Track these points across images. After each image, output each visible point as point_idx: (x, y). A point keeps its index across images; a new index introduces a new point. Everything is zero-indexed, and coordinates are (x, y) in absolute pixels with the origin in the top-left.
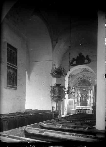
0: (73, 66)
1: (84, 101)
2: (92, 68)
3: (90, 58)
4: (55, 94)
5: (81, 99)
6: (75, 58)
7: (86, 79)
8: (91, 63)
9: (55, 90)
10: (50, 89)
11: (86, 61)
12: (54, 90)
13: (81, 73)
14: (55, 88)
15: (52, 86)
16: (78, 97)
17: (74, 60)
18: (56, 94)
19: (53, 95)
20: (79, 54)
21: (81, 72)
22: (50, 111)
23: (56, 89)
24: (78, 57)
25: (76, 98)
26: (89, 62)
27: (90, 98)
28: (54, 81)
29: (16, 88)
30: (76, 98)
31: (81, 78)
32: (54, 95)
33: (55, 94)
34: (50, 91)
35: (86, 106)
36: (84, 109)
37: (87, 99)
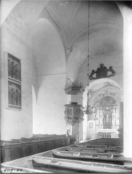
0: (93, 80)
1: (107, 122)
2: (117, 82)
3: (114, 69)
4: (70, 115)
5: (104, 120)
6: (96, 70)
7: (109, 95)
8: (115, 75)
9: (70, 110)
10: (64, 109)
11: (109, 73)
12: (69, 109)
13: (104, 88)
14: (70, 108)
15: (66, 105)
16: (99, 117)
17: (93, 72)
18: (71, 115)
19: (68, 116)
20: (100, 65)
21: (104, 87)
22: (65, 136)
23: (72, 108)
24: (98, 69)
25: (98, 119)
26: (113, 75)
27: (115, 119)
28: (69, 99)
29: (20, 108)
30: (98, 119)
31: (104, 95)
32: (69, 116)
33: (70, 115)
34: (64, 111)
35: (111, 128)
36: (107, 133)
37: (111, 120)
